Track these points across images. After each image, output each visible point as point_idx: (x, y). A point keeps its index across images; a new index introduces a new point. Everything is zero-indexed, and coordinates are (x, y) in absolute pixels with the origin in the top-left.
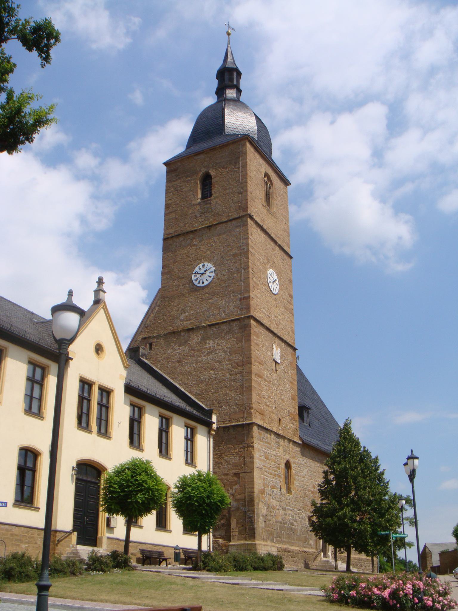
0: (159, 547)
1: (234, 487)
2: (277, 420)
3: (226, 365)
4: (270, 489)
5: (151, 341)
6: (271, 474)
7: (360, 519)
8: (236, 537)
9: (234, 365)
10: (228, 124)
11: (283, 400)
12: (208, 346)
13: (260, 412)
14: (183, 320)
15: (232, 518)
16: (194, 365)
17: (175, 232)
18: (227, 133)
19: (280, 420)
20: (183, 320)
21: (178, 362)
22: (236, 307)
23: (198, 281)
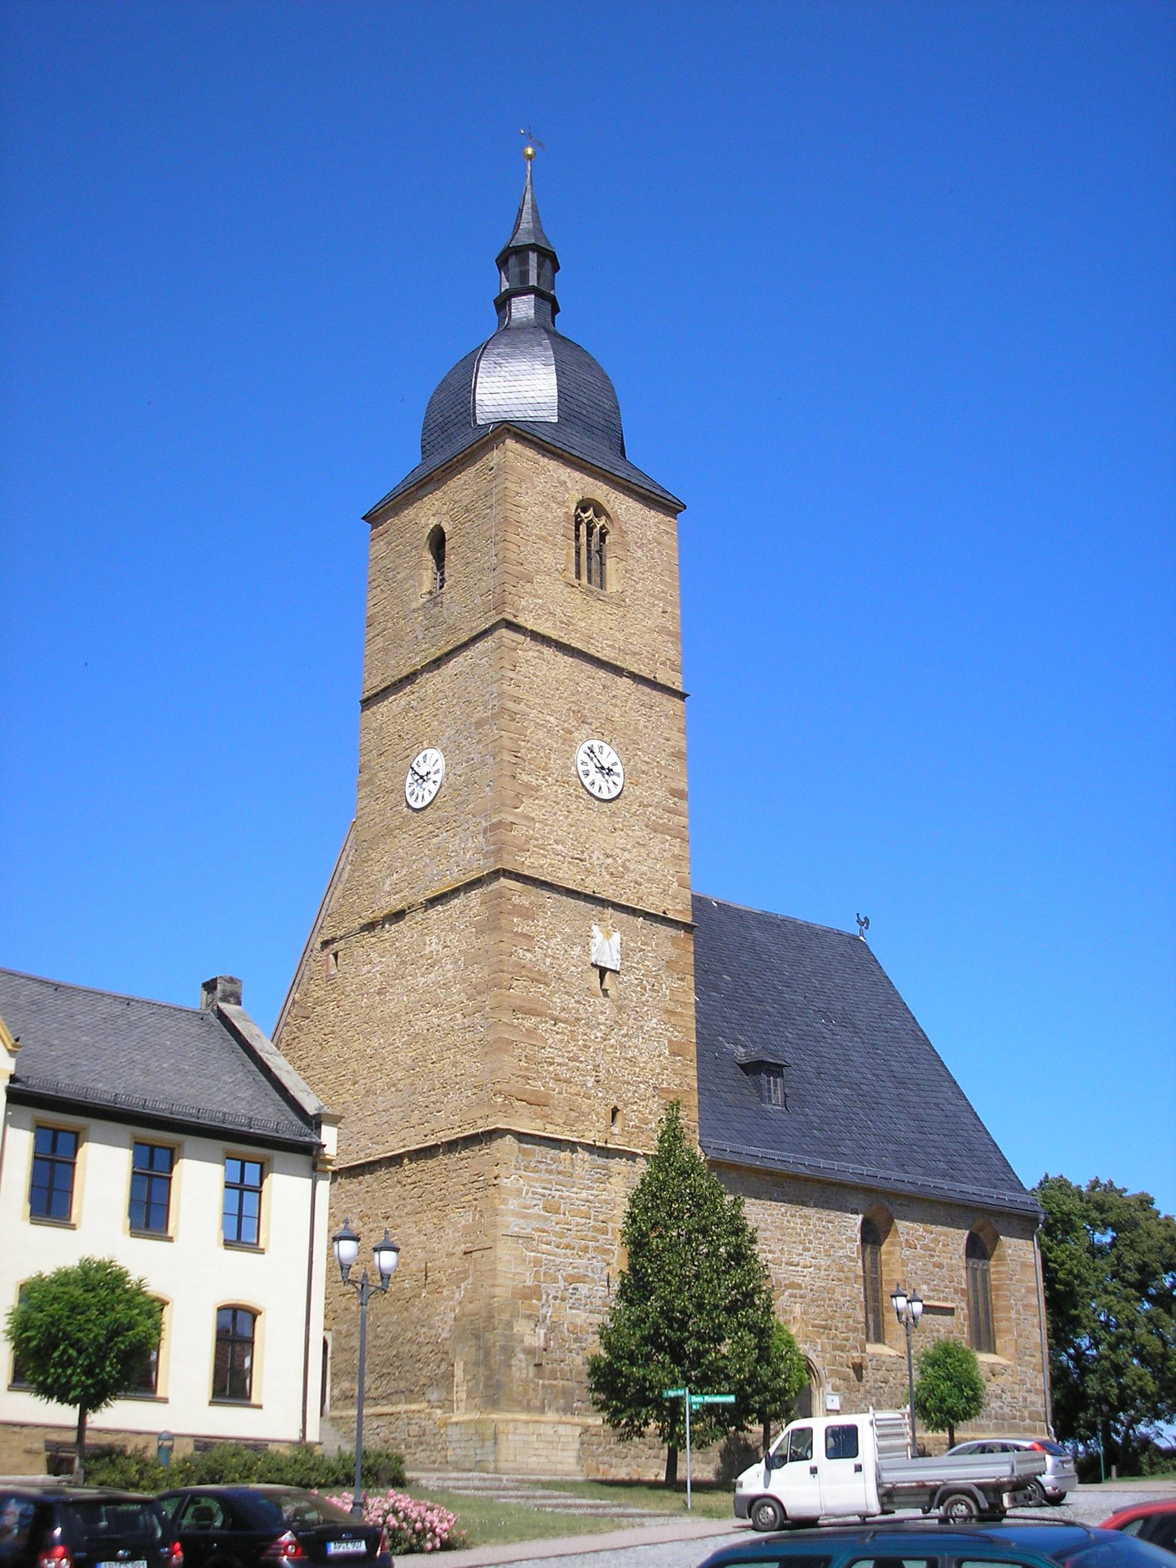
0: (120, 1436)
1: (463, 1286)
2: (605, 1112)
3: (458, 994)
4: (562, 1284)
5: (335, 946)
6: (567, 1247)
7: (696, 1350)
8: (462, 1405)
9: (471, 991)
10: (483, 397)
11: (632, 1061)
12: (428, 950)
13: (532, 1099)
14: (389, 894)
15: (458, 1359)
16: (405, 999)
17: (383, 681)
18: (479, 422)
19: (615, 1111)
20: (389, 894)
21: (379, 993)
22: (478, 850)
23: (414, 796)
